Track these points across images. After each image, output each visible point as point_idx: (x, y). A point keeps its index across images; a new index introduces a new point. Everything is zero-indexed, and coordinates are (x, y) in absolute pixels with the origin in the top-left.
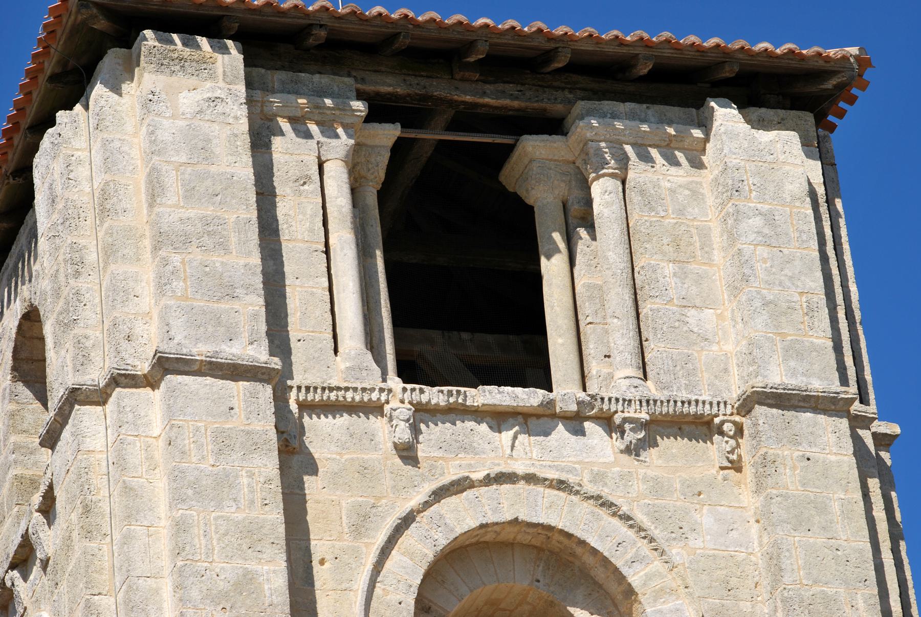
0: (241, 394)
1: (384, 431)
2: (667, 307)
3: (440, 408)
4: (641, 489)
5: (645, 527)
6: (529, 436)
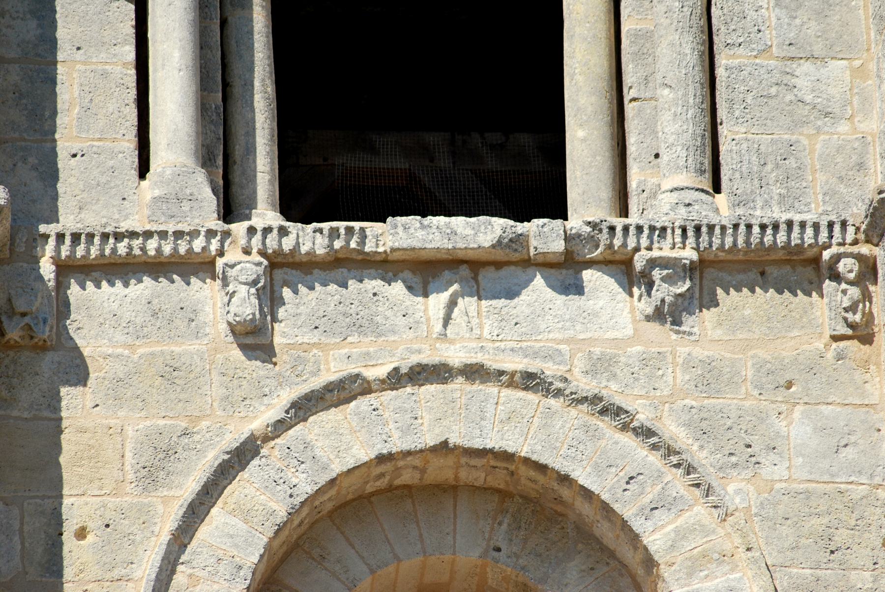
1: (214, 304)
2: (757, 61)
3: (318, 259)
4: (678, 381)
5: (677, 446)
6: (480, 299)
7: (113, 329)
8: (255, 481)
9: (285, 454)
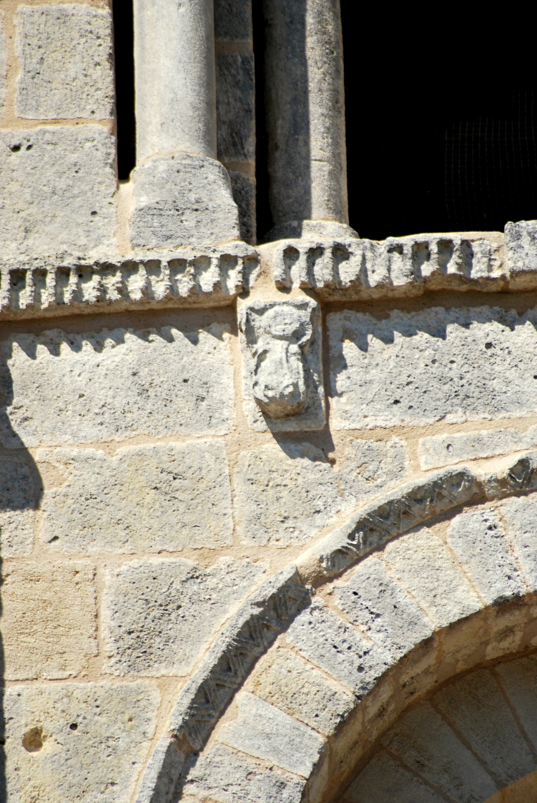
3: (397, 294)
7: (78, 418)
8: (303, 647)
9: (350, 603)
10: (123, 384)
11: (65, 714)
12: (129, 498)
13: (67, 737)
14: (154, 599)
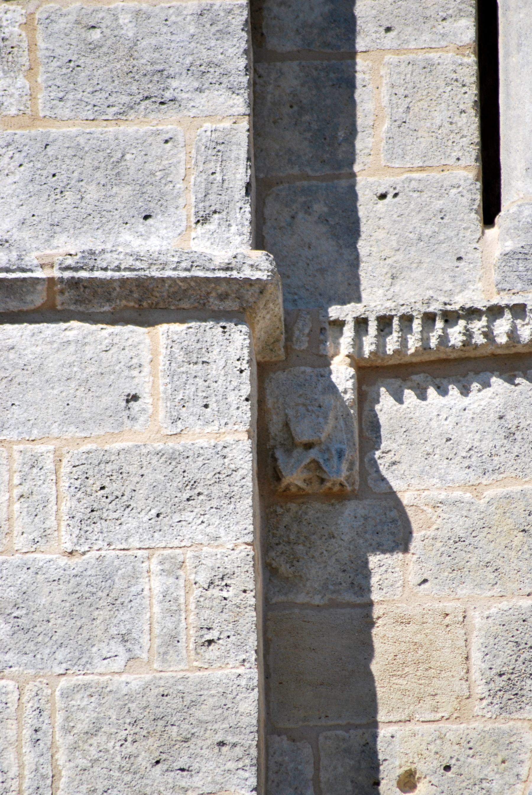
0: (161, 358)
10: (490, 428)
11: (438, 756)
12: (498, 541)
13: (441, 778)
14: (524, 642)
